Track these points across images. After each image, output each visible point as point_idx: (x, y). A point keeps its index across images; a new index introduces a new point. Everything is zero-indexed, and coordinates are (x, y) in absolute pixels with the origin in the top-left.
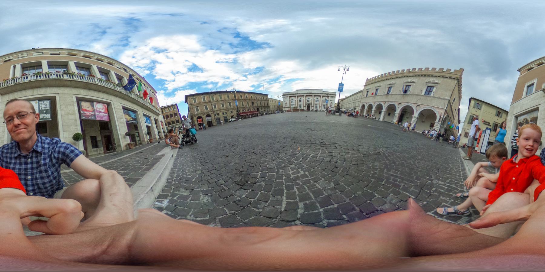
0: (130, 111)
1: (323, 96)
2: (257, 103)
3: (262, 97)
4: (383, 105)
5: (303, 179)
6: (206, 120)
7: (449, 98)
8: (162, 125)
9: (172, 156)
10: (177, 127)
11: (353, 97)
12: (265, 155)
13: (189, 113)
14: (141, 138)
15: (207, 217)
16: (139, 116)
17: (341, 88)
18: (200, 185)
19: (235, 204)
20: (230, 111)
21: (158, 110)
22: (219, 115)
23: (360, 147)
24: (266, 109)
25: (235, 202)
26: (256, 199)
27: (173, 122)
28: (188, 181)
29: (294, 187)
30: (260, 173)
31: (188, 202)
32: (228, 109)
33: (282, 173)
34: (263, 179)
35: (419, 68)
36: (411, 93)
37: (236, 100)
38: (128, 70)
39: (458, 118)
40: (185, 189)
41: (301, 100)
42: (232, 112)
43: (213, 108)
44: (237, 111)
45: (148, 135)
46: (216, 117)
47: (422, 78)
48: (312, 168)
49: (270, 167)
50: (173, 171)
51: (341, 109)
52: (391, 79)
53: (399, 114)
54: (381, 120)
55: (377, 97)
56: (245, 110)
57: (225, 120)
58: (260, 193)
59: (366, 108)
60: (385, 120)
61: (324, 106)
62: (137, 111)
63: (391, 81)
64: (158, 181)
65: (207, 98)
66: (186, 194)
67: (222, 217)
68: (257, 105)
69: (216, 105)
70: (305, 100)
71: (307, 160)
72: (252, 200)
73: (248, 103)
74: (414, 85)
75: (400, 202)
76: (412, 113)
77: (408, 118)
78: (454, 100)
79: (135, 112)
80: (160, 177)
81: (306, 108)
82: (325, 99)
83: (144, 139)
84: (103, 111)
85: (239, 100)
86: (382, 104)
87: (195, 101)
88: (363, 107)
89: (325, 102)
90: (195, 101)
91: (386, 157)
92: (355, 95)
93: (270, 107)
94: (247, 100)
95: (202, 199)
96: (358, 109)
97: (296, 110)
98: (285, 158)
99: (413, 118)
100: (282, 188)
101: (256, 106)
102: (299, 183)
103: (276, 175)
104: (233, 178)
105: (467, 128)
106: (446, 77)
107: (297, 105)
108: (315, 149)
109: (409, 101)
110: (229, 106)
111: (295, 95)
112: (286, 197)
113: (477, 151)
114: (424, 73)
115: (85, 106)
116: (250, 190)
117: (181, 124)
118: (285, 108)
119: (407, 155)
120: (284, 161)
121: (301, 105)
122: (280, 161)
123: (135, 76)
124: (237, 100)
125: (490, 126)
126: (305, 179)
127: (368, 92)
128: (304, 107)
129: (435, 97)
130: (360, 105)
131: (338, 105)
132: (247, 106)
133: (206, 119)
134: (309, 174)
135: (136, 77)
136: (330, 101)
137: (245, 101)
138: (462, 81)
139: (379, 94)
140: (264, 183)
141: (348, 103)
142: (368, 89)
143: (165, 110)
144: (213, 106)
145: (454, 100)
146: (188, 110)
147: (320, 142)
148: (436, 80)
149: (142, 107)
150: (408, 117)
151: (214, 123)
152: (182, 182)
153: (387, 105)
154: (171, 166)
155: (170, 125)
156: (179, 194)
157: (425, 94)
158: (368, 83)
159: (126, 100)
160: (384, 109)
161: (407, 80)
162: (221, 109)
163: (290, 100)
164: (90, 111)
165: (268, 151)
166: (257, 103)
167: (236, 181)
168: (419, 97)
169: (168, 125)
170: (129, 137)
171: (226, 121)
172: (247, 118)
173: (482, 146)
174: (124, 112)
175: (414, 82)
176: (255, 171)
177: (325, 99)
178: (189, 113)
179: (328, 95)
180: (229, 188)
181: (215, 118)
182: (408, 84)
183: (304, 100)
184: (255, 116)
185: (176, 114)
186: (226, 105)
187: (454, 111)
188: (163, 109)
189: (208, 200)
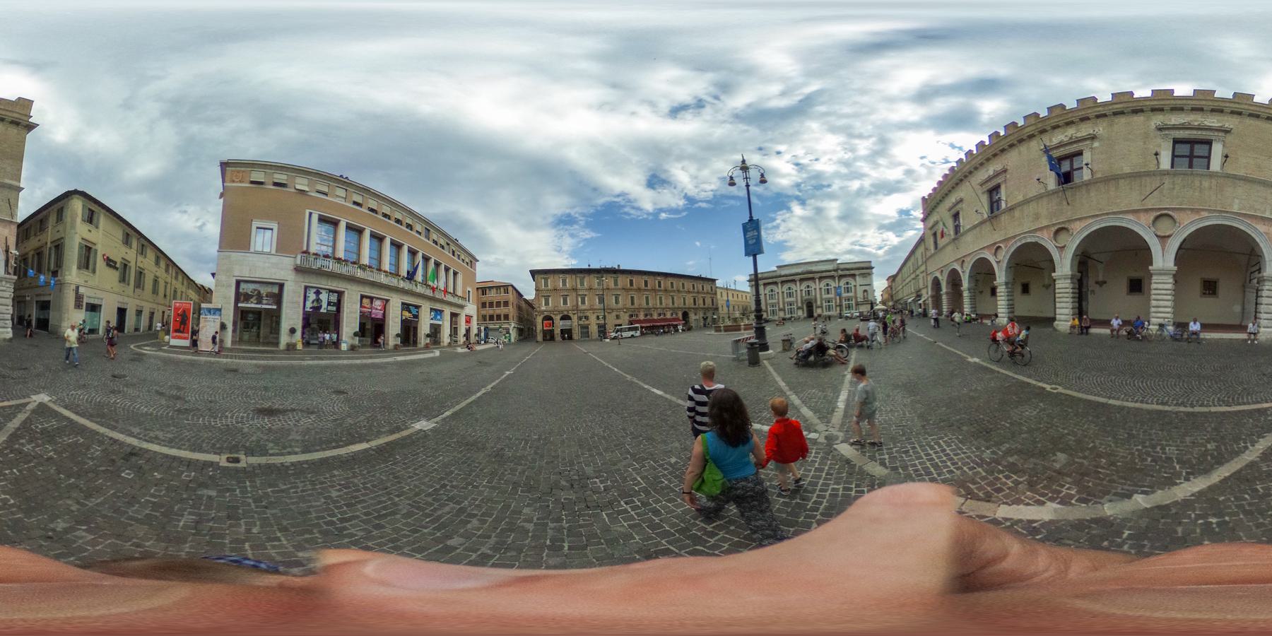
2: (684, 298)
3: (699, 286)
4: (992, 259)
6: (560, 325)
11: (910, 264)
20: (614, 314)
22: (588, 319)
27: (499, 317)
42: (618, 317)
46: (581, 322)
55: (963, 239)
56: (651, 315)
63: (988, 170)
68: (685, 304)
69: (586, 299)
70: (799, 291)
73: (660, 298)
81: (803, 311)
87: (546, 285)
90: (546, 285)
93: (720, 309)
94: (660, 291)
101: (680, 306)
110: (614, 302)
111: (774, 280)
121: (773, 306)
128: (798, 308)
130: (927, 281)
133: (561, 324)
136: (861, 285)
137: (654, 294)
144: (580, 300)
150: (1101, 279)
153: (1005, 255)
160: (1001, 278)
162: (595, 307)
163: (767, 292)
171: (603, 332)
175: (1093, 138)
183: (796, 291)
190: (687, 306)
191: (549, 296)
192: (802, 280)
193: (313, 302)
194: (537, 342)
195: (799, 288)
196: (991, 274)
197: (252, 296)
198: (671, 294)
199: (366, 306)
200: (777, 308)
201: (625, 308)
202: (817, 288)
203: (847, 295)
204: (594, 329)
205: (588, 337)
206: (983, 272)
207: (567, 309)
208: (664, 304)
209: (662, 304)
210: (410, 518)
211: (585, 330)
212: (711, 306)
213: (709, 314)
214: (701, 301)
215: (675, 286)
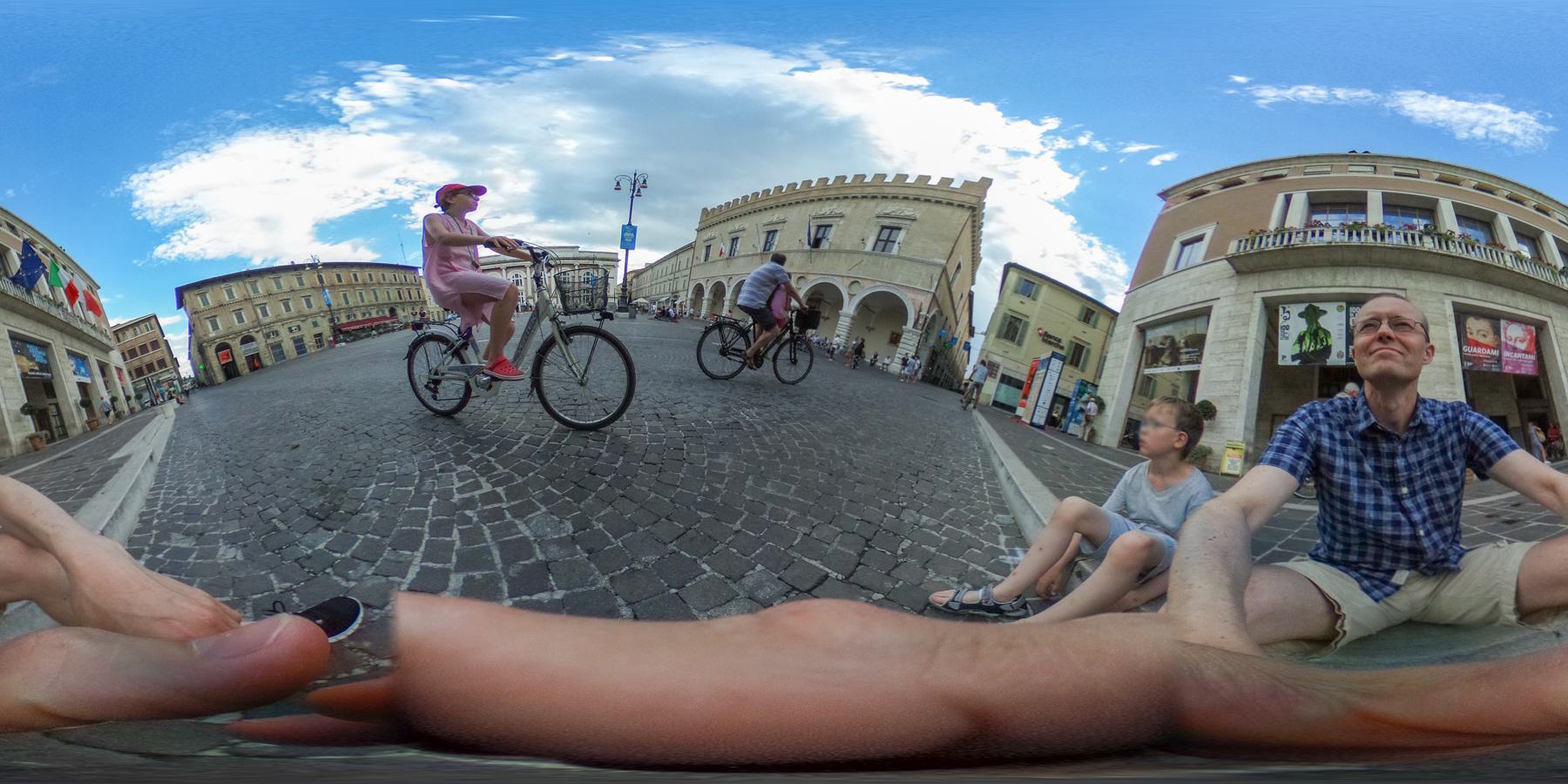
0: (31, 343)
2: (388, 292)
3: (400, 275)
5: (485, 508)
7: (945, 262)
8: (120, 379)
9: (151, 457)
12: (398, 439)
13: (193, 339)
14: (65, 419)
15: (228, 595)
16: (54, 358)
17: (629, 237)
18: (220, 522)
19: (297, 565)
21: (107, 336)
22: (278, 335)
23: (679, 407)
25: (297, 560)
26: (348, 554)
27: (150, 367)
28: (192, 514)
29: (452, 529)
30: (373, 486)
31: (189, 563)
33: (430, 489)
34: (379, 502)
35: (857, 176)
36: (832, 248)
38: (18, 227)
39: (967, 319)
40: (183, 534)
41: (519, 278)
42: (315, 324)
43: (257, 317)
44: (332, 320)
45: (83, 410)
46: (269, 341)
47: (864, 203)
48: (519, 475)
49: (403, 470)
50: (153, 495)
51: (635, 299)
52: (771, 208)
55: (736, 261)
58: (363, 540)
59: (707, 294)
62: (50, 344)
64: (117, 518)
65: (238, 290)
66: (186, 544)
67: (260, 596)
69: (268, 308)
71: (509, 453)
72: (338, 555)
73: (361, 294)
74: (841, 222)
76: (838, 303)
78: (959, 267)
79: (44, 346)
80: (121, 507)
83: (72, 421)
85: (332, 286)
87: (205, 302)
90: (205, 302)
91: (757, 435)
92: (673, 260)
95: (223, 555)
96: (685, 297)
98: (448, 447)
99: (841, 318)
100: (420, 529)
102: (471, 518)
103: (413, 493)
104: (303, 500)
105: (994, 349)
106: (937, 202)
108: (541, 418)
110: (305, 306)
111: (497, 266)
112: (424, 553)
113: (1020, 417)
114: (869, 189)
116: (340, 531)
119: (822, 428)
120: (444, 454)
122: (434, 453)
123: (37, 243)
124: (329, 287)
125: (1062, 348)
126: (490, 507)
131: (624, 289)
132: (361, 304)
133: (243, 350)
134: (506, 495)
135: (42, 247)
138: (983, 214)
139: (743, 254)
140: (377, 514)
144: (259, 311)
145: (959, 267)
147: (561, 396)
148: (908, 209)
149: (61, 331)
150: (871, 325)
151: (267, 359)
152: (179, 518)
154: (148, 481)
155: (144, 375)
156: (169, 547)
157: (874, 250)
159: (18, 313)
161: (821, 211)
165: (408, 428)
166: (388, 292)
167: (309, 508)
168: (857, 258)
169: (138, 377)
170: (33, 419)
172: (362, 338)
173: (1036, 406)
174: (13, 347)
175: (842, 216)
176: (362, 483)
178: (193, 339)
179: (596, 262)
180: (289, 527)
181: (267, 345)
182: (823, 220)
184: (385, 332)
185: (155, 345)
187: (956, 297)
188: (119, 331)
189: (235, 557)
190: (393, 300)
191: (215, 316)
193: (1301, 339)
197: (1162, 351)
199: (1481, 340)
200: (524, 296)
201: (322, 311)
204: (289, 346)
205: (285, 358)
210: (161, 553)
211: (278, 350)
212: (418, 299)
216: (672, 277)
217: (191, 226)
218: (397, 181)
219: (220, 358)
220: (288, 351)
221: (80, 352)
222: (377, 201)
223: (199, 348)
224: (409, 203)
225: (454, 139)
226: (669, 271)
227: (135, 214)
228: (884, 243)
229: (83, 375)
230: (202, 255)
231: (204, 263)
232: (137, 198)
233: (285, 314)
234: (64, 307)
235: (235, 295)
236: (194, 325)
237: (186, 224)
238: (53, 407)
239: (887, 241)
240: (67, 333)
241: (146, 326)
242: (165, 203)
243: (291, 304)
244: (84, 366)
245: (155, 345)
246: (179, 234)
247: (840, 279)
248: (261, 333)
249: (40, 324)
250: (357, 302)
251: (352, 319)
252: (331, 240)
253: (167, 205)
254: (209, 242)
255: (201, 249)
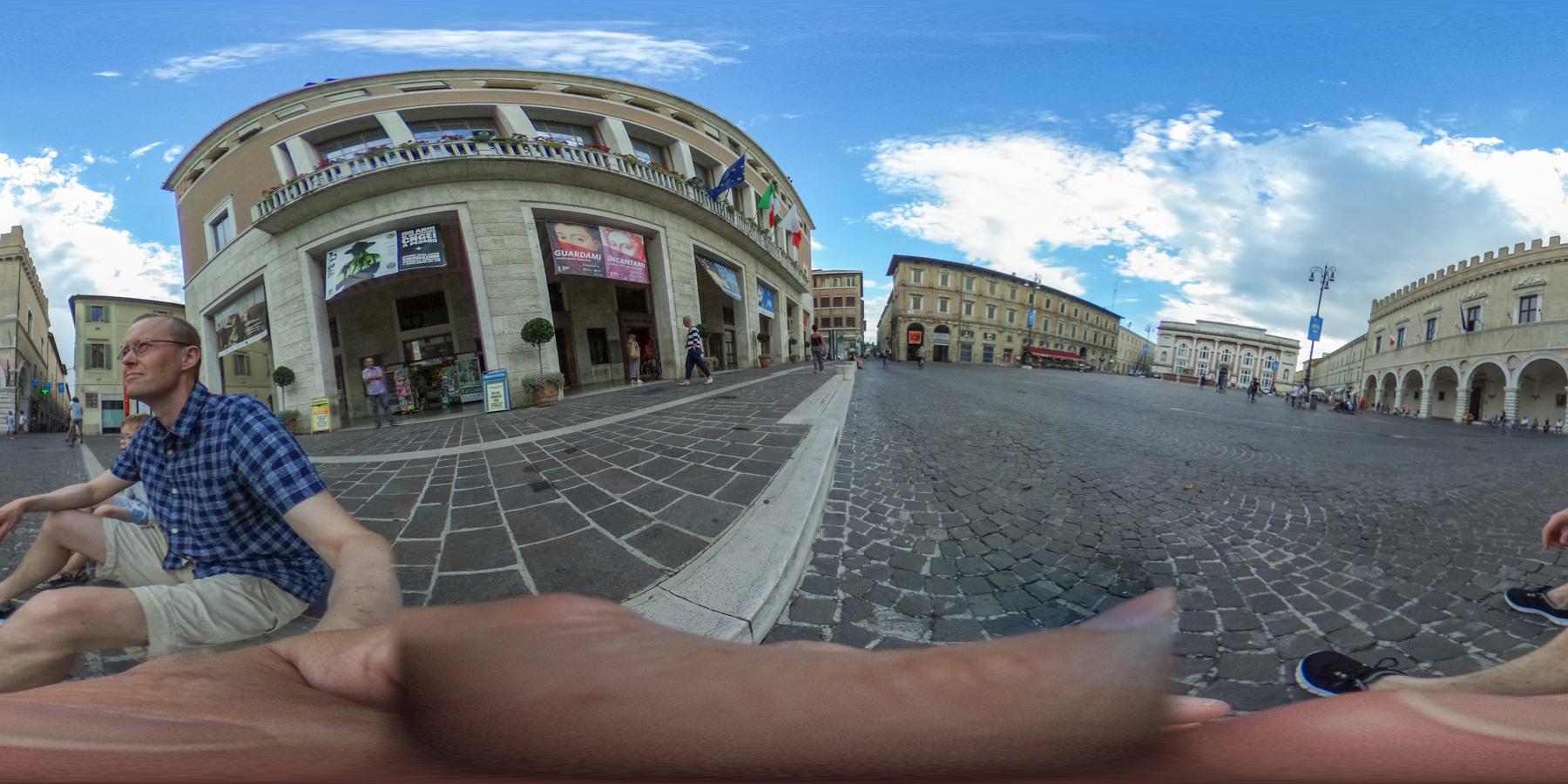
1: (1265, 349)
2: (1086, 332)
3: (1103, 319)
8: (805, 323)
10: (845, 336)
14: (739, 348)
21: (805, 278)
22: (972, 336)
24: (1106, 357)
27: (838, 321)
32: (1002, 328)
36: (1485, 328)
37: (1032, 309)
42: (1010, 339)
46: (962, 339)
53: (1467, 391)
54: (1423, 414)
55: (1403, 352)
56: (1048, 344)
57: (985, 355)
59: (1379, 386)
60: (1435, 414)
61: (1265, 378)
62: (741, 268)
63: (1430, 303)
65: (953, 280)
68: (1085, 338)
69: (973, 307)
70: (1215, 354)
73: (1061, 325)
74: (1487, 302)
75: (1526, 575)
76: (1501, 380)
77: (1494, 396)
82: (1270, 358)
83: (745, 353)
84: (631, 253)
85: (1039, 309)
86: (1420, 369)
87: (917, 279)
88: (1371, 381)
89: (1269, 367)
90: (917, 279)
92: (1348, 351)
94: (1062, 316)
96: (1359, 390)
97: (1187, 377)
99: (1507, 394)
101: (1080, 340)
107: (1191, 365)
109: (1485, 351)
111: (1191, 334)
115: (568, 236)
117: (857, 332)
118: (1158, 365)
121: (1246, 373)
127: (1379, 339)
129: (1548, 323)
130: (1362, 377)
132: (1057, 335)
135: (764, 171)
139: (1409, 344)
141: (1330, 373)
142: (1379, 331)
143: (823, 281)
144: (964, 307)
146: (891, 297)
148: (1536, 276)
150: (1492, 394)
151: (954, 356)
153: (1431, 371)
155: (829, 326)
157: (1520, 321)
158: (1379, 314)
160: (1427, 385)
164: (586, 251)
166: (1086, 332)
172: (1047, 368)
177: (1270, 358)
181: (959, 342)
184: (1070, 369)
185: (851, 301)
186: (1000, 315)
188: (819, 277)
191: (921, 296)
192: (1222, 342)
194: (899, 361)
195: (1216, 351)
196: (1420, 383)
198: (1074, 323)
201: (1021, 330)
202: (1236, 355)
203: (1245, 366)
204: (978, 350)
205: (970, 360)
206: (1414, 380)
207: (945, 317)
208: (1063, 334)
209: (1061, 334)
211: (966, 351)
212: (1110, 347)
213: (1106, 357)
214: (1102, 339)
215: (1078, 314)
216: (1347, 368)
217: (919, 203)
218: (1127, 224)
219: (910, 337)
220: (975, 355)
221: (771, 285)
222: (1101, 237)
223: (893, 320)
224: (1128, 248)
225: (1192, 192)
226: (1345, 363)
227: (866, 175)
228: (1527, 313)
229: (768, 309)
230: (918, 234)
231: (917, 241)
232: (876, 161)
233: (986, 319)
234: (769, 235)
235: (949, 283)
236: (896, 297)
237: (915, 200)
238: (728, 334)
239: (1529, 310)
240: (762, 263)
241: (849, 281)
242: (904, 174)
243: (995, 312)
244: (772, 300)
245: (851, 301)
246: (904, 207)
247: (1497, 357)
248: (957, 328)
249: (734, 246)
250: (1055, 332)
251: (1044, 346)
252: (1046, 262)
253: (905, 176)
254: (931, 224)
255: (920, 229)
